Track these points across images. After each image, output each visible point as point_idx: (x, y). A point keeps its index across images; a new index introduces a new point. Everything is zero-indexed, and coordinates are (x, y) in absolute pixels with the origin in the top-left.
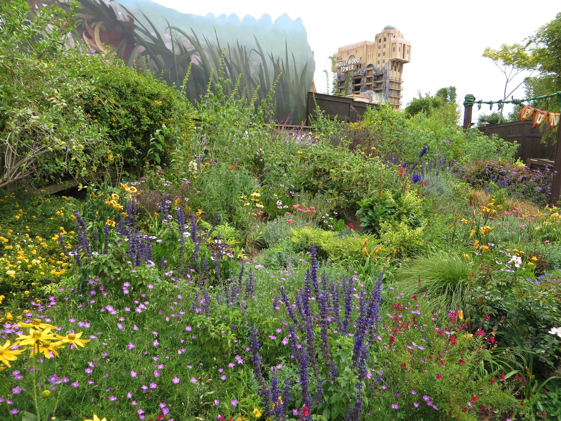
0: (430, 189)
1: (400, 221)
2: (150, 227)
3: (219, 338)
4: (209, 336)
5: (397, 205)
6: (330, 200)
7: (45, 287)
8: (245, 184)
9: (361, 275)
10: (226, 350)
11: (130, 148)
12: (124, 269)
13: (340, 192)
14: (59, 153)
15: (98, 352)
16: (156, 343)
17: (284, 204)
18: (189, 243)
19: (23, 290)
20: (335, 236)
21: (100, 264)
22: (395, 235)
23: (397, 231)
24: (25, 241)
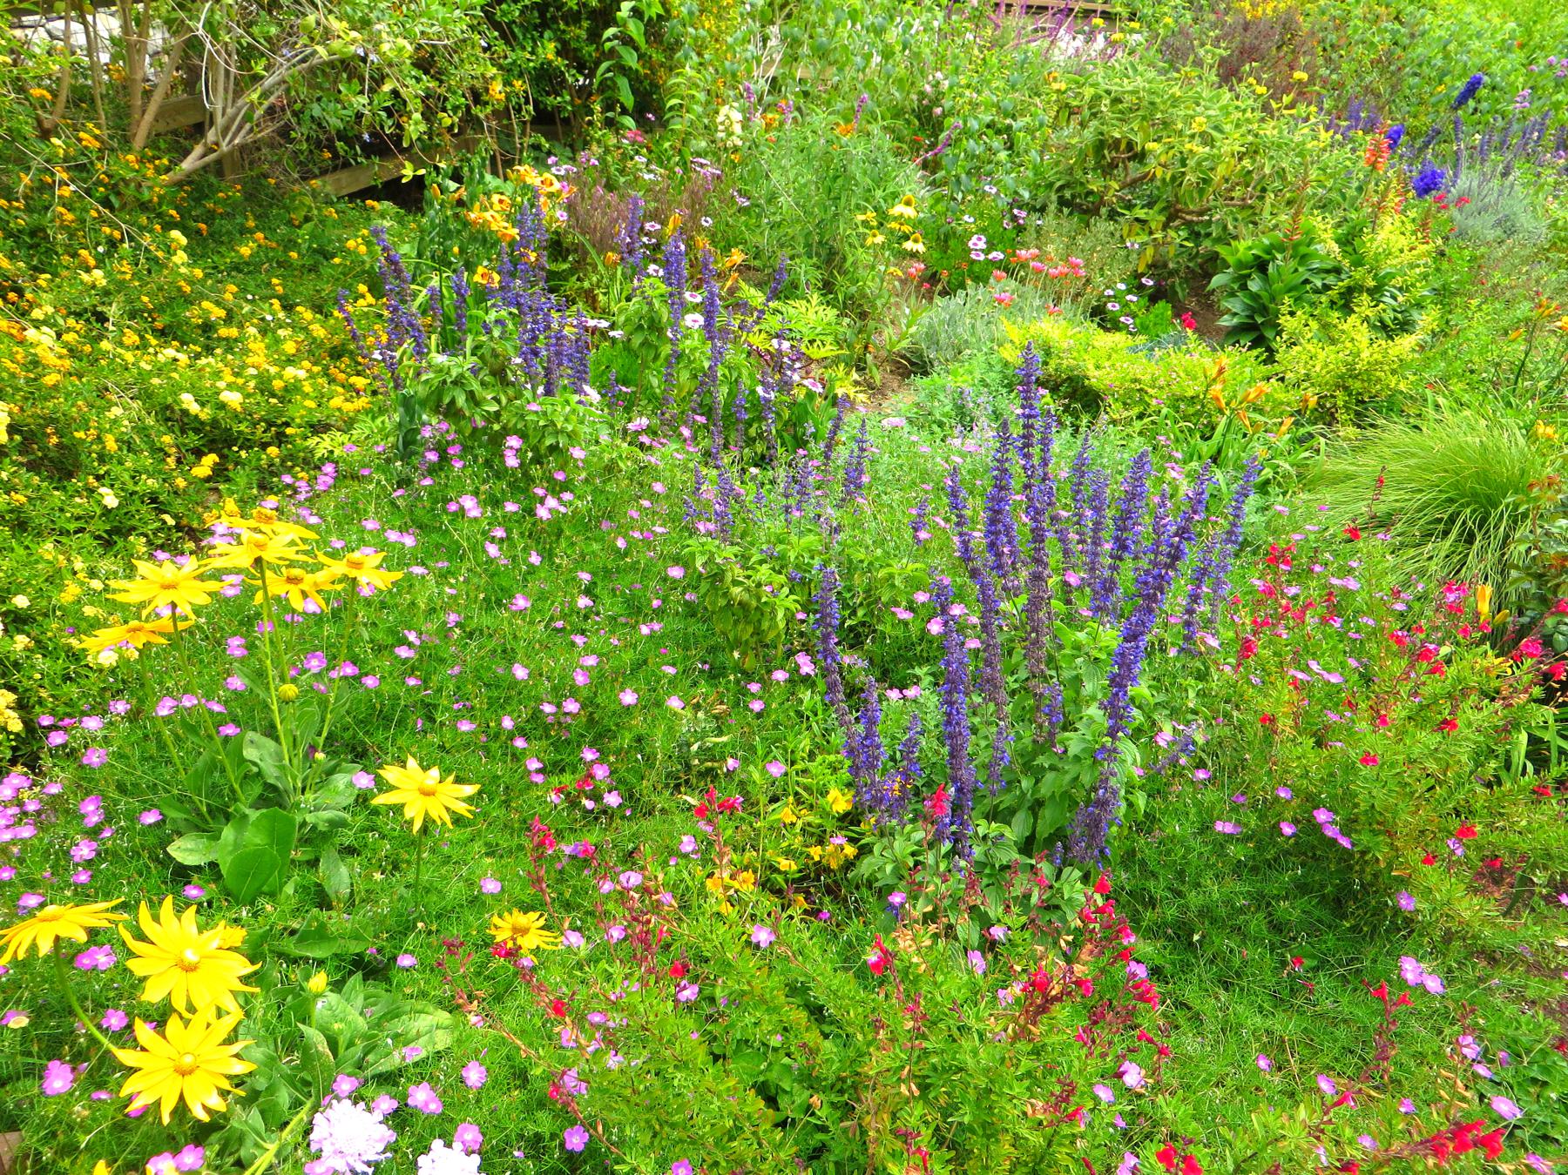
0: (1470, 222)
1: (1347, 309)
2: (601, 297)
3: (754, 603)
4: (725, 594)
5: (1346, 263)
6: (1135, 242)
7: (317, 439)
8: (879, 181)
9: (1194, 465)
10: (771, 635)
11: (550, 63)
12: (510, 400)
13: (1170, 219)
14: (348, 67)
15: (432, 611)
16: (583, 602)
17: (991, 246)
18: (696, 343)
19: (264, 446)
20: (1134, 350)
21: (444, 382)
22: (1322, 355)
23: (1333, 342)
24: (269, 318)
